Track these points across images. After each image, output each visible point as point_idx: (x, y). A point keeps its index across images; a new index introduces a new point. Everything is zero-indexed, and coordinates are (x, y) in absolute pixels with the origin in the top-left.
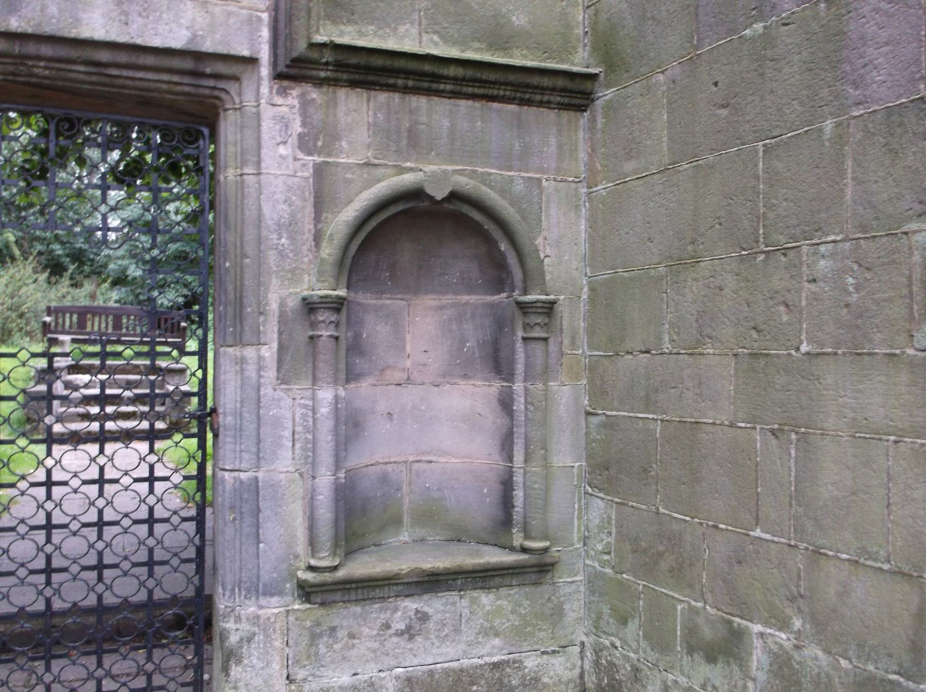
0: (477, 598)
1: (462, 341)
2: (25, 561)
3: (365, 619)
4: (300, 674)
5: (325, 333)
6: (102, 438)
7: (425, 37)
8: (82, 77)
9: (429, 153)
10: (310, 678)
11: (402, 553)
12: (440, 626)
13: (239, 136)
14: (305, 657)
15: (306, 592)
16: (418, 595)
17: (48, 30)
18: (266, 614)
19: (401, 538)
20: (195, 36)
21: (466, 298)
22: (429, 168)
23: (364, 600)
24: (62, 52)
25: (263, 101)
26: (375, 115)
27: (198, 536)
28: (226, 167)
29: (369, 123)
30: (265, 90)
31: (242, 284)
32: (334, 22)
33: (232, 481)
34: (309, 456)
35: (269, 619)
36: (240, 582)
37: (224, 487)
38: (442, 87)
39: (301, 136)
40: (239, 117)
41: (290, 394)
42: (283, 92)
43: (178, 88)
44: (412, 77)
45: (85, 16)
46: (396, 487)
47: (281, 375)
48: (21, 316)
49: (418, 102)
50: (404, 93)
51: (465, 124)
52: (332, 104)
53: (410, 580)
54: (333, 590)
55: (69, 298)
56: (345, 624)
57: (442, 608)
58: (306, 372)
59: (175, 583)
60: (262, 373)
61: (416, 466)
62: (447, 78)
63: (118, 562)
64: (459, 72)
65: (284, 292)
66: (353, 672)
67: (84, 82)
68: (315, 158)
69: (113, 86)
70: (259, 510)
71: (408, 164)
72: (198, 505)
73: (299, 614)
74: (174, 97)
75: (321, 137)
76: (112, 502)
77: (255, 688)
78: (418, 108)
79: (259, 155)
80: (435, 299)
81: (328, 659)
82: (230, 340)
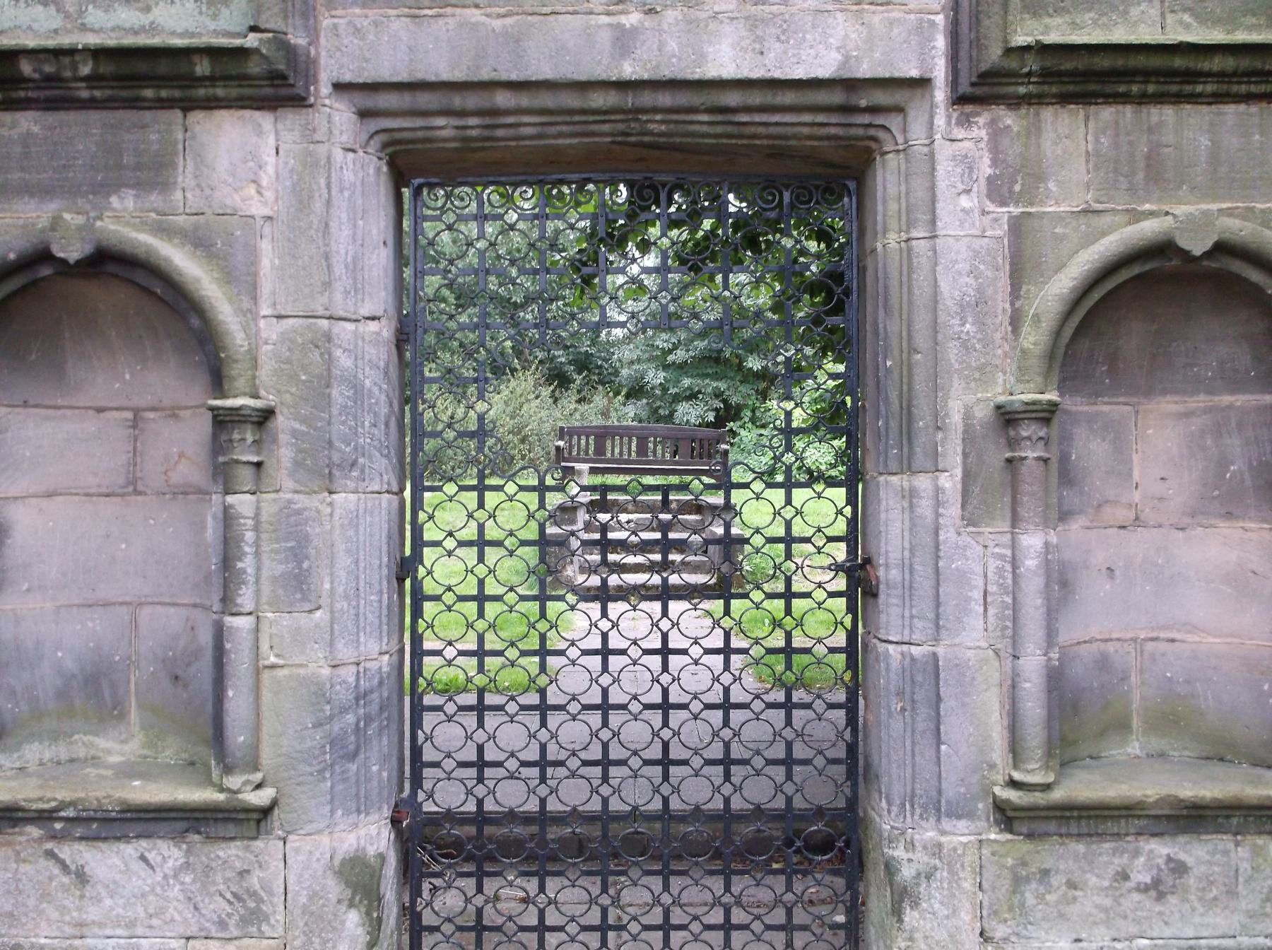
0: (1262, 848)
1: (1223, 464)
2: (516, 749)
3: (1091, 863)
4: (1000, 931)
5: (1031, 453)
6: (665, 594)
7: (1170, 19)
8: (705, 129)
9: (1180, 187)
10: (1013, 939)
11: (1132, 772)
12: (1204, 884)
13: (903, 188)
14: (1005, 908)
15: (1006, 816)
16: (1170, 834)
17: (667, 73)
18: (951, 842)
19: (1129, 750)
20: (847, 58)
21: (1227, 399)
22: (1180, 210)
23: (1090, 835)
24: (683, 99)
25: (938, 136)
26: (1097, 141)
27: (849, 729)
28: (885, 232)
29: (1087, 152)
30: (940, 121)
31: (910, 389)
32: (1035, 15)
33: (899, 656)
34: (1007, 627)
35: (955, 849)
36: (913, 797)
37: (888, 664)
38: (1199, 88)
39: (990, 180)
40: (902, 161)
41: (980, 539)
42: (965, 121)
43: (823, 131)
44: (1153, 79)
45: (710, 50)
46: (1120, 675)
47: (966, 514)
48: (523, 441)
49: (1161, 115)
50: (1140, 104)
51: (1234, 140)
52: (1035, 130)
53: (1160, 812)
54: (1047, 818)
55: (577, 416)
56: (1061, 867)
57: (1208, 857)
58: (1001, 509)
59: (818, 790)
60: (941, 510)
61: (1150, 646)
62: (1209, 74)
63: (503, 759)
64: (1229, 63)
65: (970, 398)
66: (1075, 936)
67: (704, 135)
68: (1011, 209)
69: (742, 137)
70: (939, 698)
71: (1147, 206)
72: (848, 688)
73: (996, 847)
74: (816, 143)
75: (1019, 178)
76: (740, 679)
77: (938, 943)
78: (1161, 124)
79: (933, 211)
80: (1176, 403)
81: (1039, 915)
82: (893, 466)
